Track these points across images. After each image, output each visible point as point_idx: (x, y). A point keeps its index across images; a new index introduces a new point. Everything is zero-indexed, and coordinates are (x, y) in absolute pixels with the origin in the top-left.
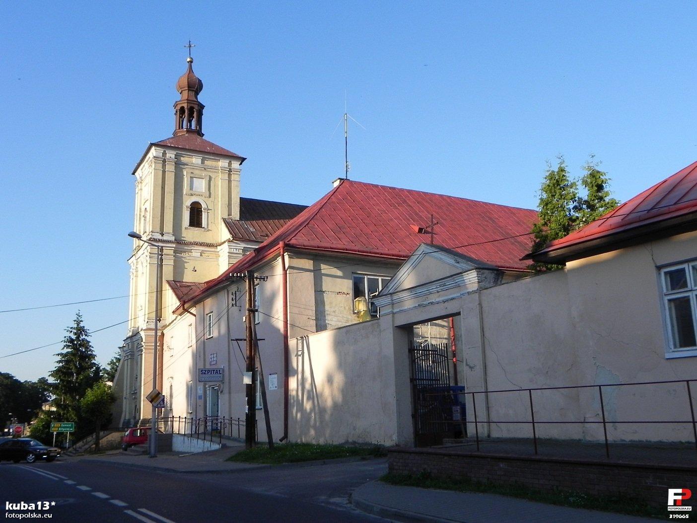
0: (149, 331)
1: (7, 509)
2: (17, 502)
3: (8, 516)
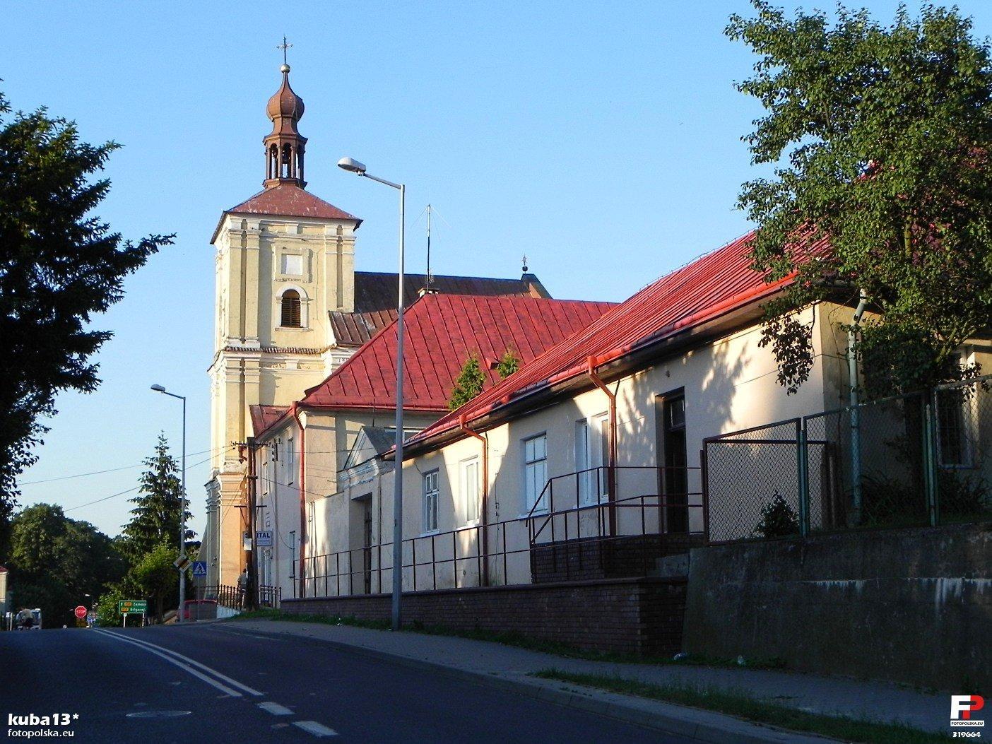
0: (227, 476)
1: (10, 724)
2: (25, 714)
3: (11, 733)
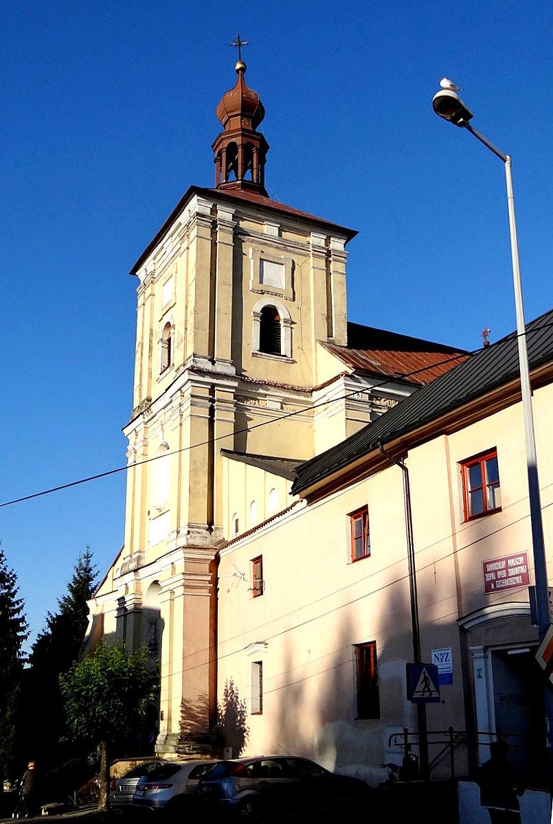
0: (192, 551)
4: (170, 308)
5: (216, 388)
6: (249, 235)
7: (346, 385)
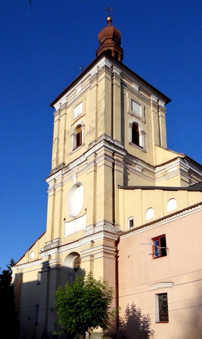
4: (81, 117)
5: (115, 154)
6: (127, 86)
7: (180, 163)
